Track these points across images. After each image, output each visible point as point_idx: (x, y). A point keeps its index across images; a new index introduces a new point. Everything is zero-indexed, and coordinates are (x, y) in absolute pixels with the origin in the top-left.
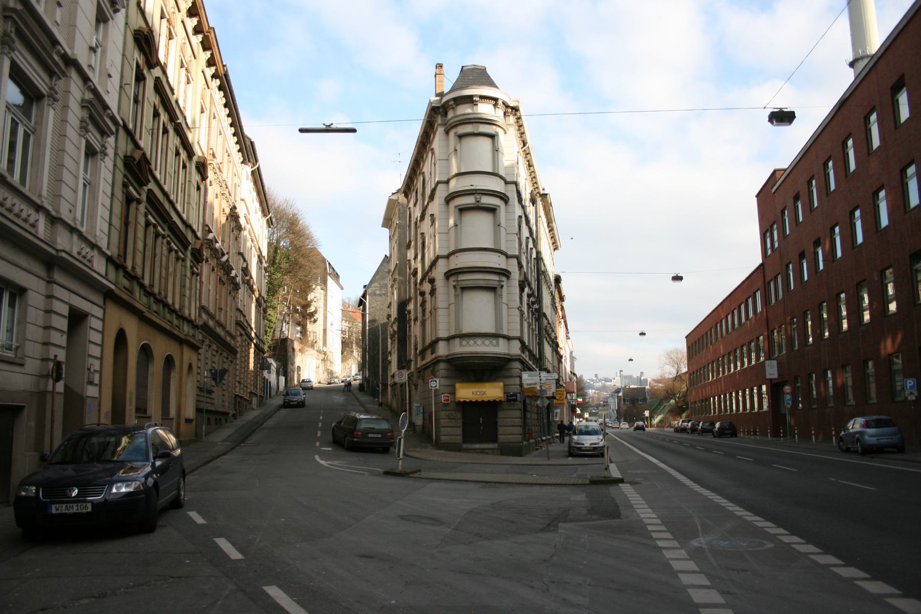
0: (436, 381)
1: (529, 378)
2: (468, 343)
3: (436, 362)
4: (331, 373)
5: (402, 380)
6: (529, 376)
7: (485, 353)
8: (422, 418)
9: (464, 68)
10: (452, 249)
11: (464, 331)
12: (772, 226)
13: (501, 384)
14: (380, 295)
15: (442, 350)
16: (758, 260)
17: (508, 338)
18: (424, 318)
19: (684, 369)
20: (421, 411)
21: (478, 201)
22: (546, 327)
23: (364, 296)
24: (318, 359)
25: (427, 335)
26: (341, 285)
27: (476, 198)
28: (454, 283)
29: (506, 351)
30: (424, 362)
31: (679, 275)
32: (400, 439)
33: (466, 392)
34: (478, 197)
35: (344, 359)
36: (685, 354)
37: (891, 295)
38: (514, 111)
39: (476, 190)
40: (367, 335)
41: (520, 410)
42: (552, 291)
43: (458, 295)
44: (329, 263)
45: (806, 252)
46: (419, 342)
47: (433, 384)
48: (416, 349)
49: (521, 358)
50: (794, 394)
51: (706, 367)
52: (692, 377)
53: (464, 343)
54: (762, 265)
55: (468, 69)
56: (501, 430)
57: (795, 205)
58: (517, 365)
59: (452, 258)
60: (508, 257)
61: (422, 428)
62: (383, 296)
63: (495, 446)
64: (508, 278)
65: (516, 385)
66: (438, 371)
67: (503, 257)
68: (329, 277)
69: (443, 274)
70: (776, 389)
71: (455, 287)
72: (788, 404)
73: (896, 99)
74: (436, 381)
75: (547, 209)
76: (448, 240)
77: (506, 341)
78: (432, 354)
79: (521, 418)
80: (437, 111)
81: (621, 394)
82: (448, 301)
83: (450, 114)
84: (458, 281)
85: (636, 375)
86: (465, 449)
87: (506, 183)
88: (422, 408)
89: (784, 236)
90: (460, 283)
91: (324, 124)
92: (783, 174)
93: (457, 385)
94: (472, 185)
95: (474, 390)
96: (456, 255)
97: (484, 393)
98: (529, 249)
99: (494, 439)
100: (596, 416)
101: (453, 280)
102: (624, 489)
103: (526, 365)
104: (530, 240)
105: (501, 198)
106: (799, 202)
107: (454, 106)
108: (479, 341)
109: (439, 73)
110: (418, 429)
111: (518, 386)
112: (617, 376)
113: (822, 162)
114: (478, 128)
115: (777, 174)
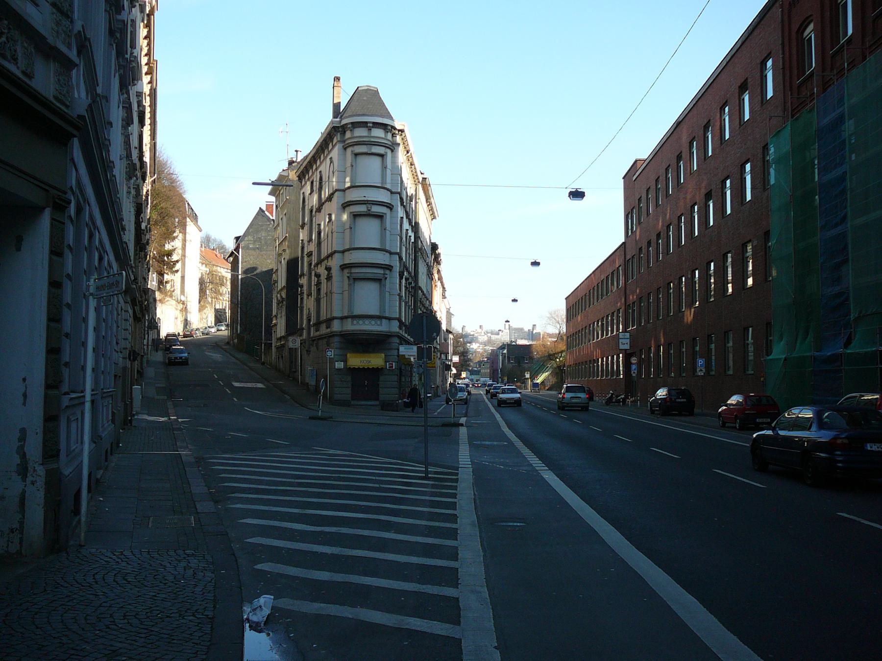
0: (331, 351)
1: (405, 350)
2: (358, 323)
3: (332, 335)
4: (186, 323)
5: (296, 345)
6: (405, 349)
7: (371, 331)
9: (359, 89)
10: (347, 247)
11: (355, 314)
12: (632, 210)
14: (254, 249)
15: (336, 326)
16: (621, 239)
17: (390, 319)
18: (319, 297)
19: (564, 330)
20: (315, 373)
21: (369, 210)
22: (421, 299)
23: (237, 249)
24: (176, 309)
25: (322, 313)
26: (199, 226)
27: (367, 207)
28: (348, 275)
29: (388, 330)
30: (318, 333)
31: (537, 261)
32: (320, 396)
33: (356, 361)
34: (369, 206)
35: (201, 309)
36: (564, 317)
37: (750, 271)
38: (400, 132)
39: (368, 201)
40: (240, 289)
41: (397, 375)
42: (428, 263)
43: (351, 284)
44: (188, 203)
45: (652, 241)
48: (309, 320)
49: (399, 334)
50: (639, 365)
52: (569, 340)
53: (355, 322)
54: (624, 243)
55: (363, 90)
58: (397, 340)
59: (346, 253)
60: (391, 253)
61: (314, 387)
62: (257, 250)
63: (377, 403)
64: (391, 270)
65: (394, 356)
66: (332, 343)
67: (388, 254)
68: (188, 219)
69: (339, 266)
70: (628, 356)
71: (348, 277)
72: (634, 373)
73: (742, 98)
74: (331, 351)
75: (426, 189)
77: (387, 321)
78: (327, 328)
79: (397, 382)
80: (337, 129)
81: (505, 351)
82: (343, 288)
83: (348, 134)
84: (351, 273)
85: (527, 327)
86: (353, 405)
87: (392, 193)
88: (315, 371)
89: (639, 222)
91: (270, 180)
92: (644, 163)
93: (348, 355)
94: (365, 197)
95: (361, 359)
96: (350, 252)
98: (408, 237)
99: (377, 399)
101: (347, 272)
103: (403, 338)
105: (387, 207)
107: (352, 129)
108: (367, 322)
109: (337, 85)
111: (396, 357)
112: (505, 329)
113: (759, 61)
114: (371, 149)
115: (638, 164)
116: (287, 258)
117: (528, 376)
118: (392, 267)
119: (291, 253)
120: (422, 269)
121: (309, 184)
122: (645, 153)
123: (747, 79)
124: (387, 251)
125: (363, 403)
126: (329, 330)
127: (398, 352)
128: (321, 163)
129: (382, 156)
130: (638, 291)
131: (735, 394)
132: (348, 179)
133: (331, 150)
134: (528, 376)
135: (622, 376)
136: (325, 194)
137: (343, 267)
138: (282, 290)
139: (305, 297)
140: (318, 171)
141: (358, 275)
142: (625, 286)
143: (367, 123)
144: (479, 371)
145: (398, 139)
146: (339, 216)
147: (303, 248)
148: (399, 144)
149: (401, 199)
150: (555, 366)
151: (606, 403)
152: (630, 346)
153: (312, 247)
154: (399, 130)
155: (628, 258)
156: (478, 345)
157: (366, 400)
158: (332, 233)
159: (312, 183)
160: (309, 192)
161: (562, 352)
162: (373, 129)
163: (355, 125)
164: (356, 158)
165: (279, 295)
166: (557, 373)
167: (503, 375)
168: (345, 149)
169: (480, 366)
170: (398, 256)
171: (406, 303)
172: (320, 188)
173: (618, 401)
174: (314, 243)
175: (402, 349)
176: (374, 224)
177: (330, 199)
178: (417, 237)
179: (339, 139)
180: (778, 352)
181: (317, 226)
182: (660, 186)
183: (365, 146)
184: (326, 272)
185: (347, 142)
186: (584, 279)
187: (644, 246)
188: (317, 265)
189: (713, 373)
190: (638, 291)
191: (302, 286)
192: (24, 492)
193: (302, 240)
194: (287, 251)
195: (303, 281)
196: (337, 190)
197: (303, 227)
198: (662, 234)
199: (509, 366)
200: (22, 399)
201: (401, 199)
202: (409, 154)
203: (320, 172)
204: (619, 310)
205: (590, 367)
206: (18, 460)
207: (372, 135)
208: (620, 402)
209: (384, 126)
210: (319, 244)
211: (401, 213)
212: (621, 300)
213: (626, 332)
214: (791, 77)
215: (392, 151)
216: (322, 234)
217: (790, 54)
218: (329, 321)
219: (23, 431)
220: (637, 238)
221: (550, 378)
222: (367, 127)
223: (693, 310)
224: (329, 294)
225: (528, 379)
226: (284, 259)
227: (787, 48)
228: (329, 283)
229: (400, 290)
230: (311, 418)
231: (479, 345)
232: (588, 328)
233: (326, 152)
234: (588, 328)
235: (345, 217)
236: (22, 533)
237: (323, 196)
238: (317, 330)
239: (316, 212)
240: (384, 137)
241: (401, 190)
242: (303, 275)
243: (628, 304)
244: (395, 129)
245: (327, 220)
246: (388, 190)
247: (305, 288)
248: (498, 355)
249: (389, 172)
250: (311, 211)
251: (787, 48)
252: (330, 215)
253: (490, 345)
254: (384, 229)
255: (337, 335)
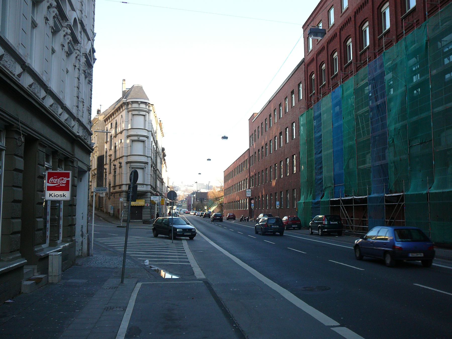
8: (113, 211)
9: (134, 86)
10: (129, 154)
13: (144, 200)
17: (147, 185)
28: (130, 166)
29: (146, 190)
31: (226, 136)
46: (112, 182)
47: (121, 200)
48: (110, 185)
51: (245, 180)
56: (143, 215)
57: (279, 108)
58: (150, 194)
59: (128, 157)
63: (142, 221)
64: (147, 164)
67: (146, 157)
70: (250, 199)
71: (130, 167)
75: (161, 125)
76: (127, 150)
77: (146, 186)
78: (119, 188)
83: (130, 106)
85: (206, 183)
87: (148, 131)
90: (131, 166)
97: (138, 203)
99: (141, 219)
100: (181, 207)
102: (118, 131)
104: (153, 142)
105: (146, 137)
106: (294, 95)
110: (112, 215)
113: (297, 84)
114: (139, 113)
116: (98, 155)
117: (206, 208)
118: (148, 163)
119: (99, 153)
120: (159, 161)
121: (110, 124)
122: (258, 109)
123: (293, 90)
124: (146, 156)
125: (135, 221)
126: (120, 189)
127: (150, 199)
128: (116, 116)
129: (144, 115)
130: (254, 171)
131: (285, 216)
132: (129, 125)
133: (122, 112)
134: (206, 208)
135: (248, 209)
136: (119, 130)
137: (127, 163)
138: (94, 170)
139: (108, 174)
140: (115, 119)
141: (134, 166)
142: (249, 168)
143: (138, 102)
144: (182, 205)
145: (151, 108)
146: (125, 141)
147: (106, 152)
148: (151, 110)
149: (152, 133)
150: (219, 203)
151: (240, 220)
152: (251, 195)
153: (112, 152)
154: (152, 105)
155: (250, 156)
156: (181, 192)
157: (136, 219)
158: (122, 148)
159: (112, 124)
160: (110, 128)
161: (222, 197)
162: (141, 104)
163: (133, 102)
164: (133, 116)
165: (93, 172)
166: (220, 207)
167: (193, 207)
168: (128, 112)
169: (182, 202)
170: (150, 158)
171: (153, 177)
172: (116, 127)
173: (245, 220)
174: (112, 151)
175: (152, 198)
176: (140, 145)
177: (121, 133)
178: (157, 147)
179: (126, 108)
180: (302, 200)
181: (114, 144)
182: (267, 122)
183: (137, 111)
184: (119, 164)
185: (129, 109)
186: (232, 163)
187: (257, 151)
188: (114, 161)
189: (282, 207)
190: (254, 171)
191: (106, 169)
192: (82, 241)
193: (106, 149)
194: (98, 152)
195: (107, 167)
196: (124, 130)
197: (106, 143)
198: (264, 147)
199: (197, 203)
200: (82, 218)
201: (152, 133)
202: (155, 113)
203: (116, 120)
204: (247, 179)
205: (234, 204)
206: (81, 233)
207: (140, 107)
208: (246, 220)
209: (145, 103)
210: (115, 151)
211: (152, 139)
212: (248, 174)
213: (249, 189)
214: (308, 93)
215: (149, 113)
216: (117, 148)
217: (307, 84)
218: (120, 186)
219: (82, 226)
220: (254, 147)
221: (217, 209)
222: (138, 103)
223: (275, 181)
224: (121, 174)
225: (206, 209)
226: (96, 156)
227: (306, 81)
228: (120, 169)
229: (151, 172)
230: (118, 227)
231: (181, 192)
232: (233, 186)
233: (119, 112)
234: (233, 186)
235: (128, 141)
236: (82, 251)
237: (117, 131)
238: (114, 189)
239: (114, 137)
240: (145, 107)
241: (152, 130)
242: (106, 164)
243: (250, 176)
244: (150, 104)
245: (120, 142)
246: (146, 130)
247: (108, 170)
248: (191, 197)
249: (147, 122)
250: (111, 136)
251: (306, 81)
252: (121, 140)
253: (187, 192)
254: (145, 147)
255: (124, 192)
